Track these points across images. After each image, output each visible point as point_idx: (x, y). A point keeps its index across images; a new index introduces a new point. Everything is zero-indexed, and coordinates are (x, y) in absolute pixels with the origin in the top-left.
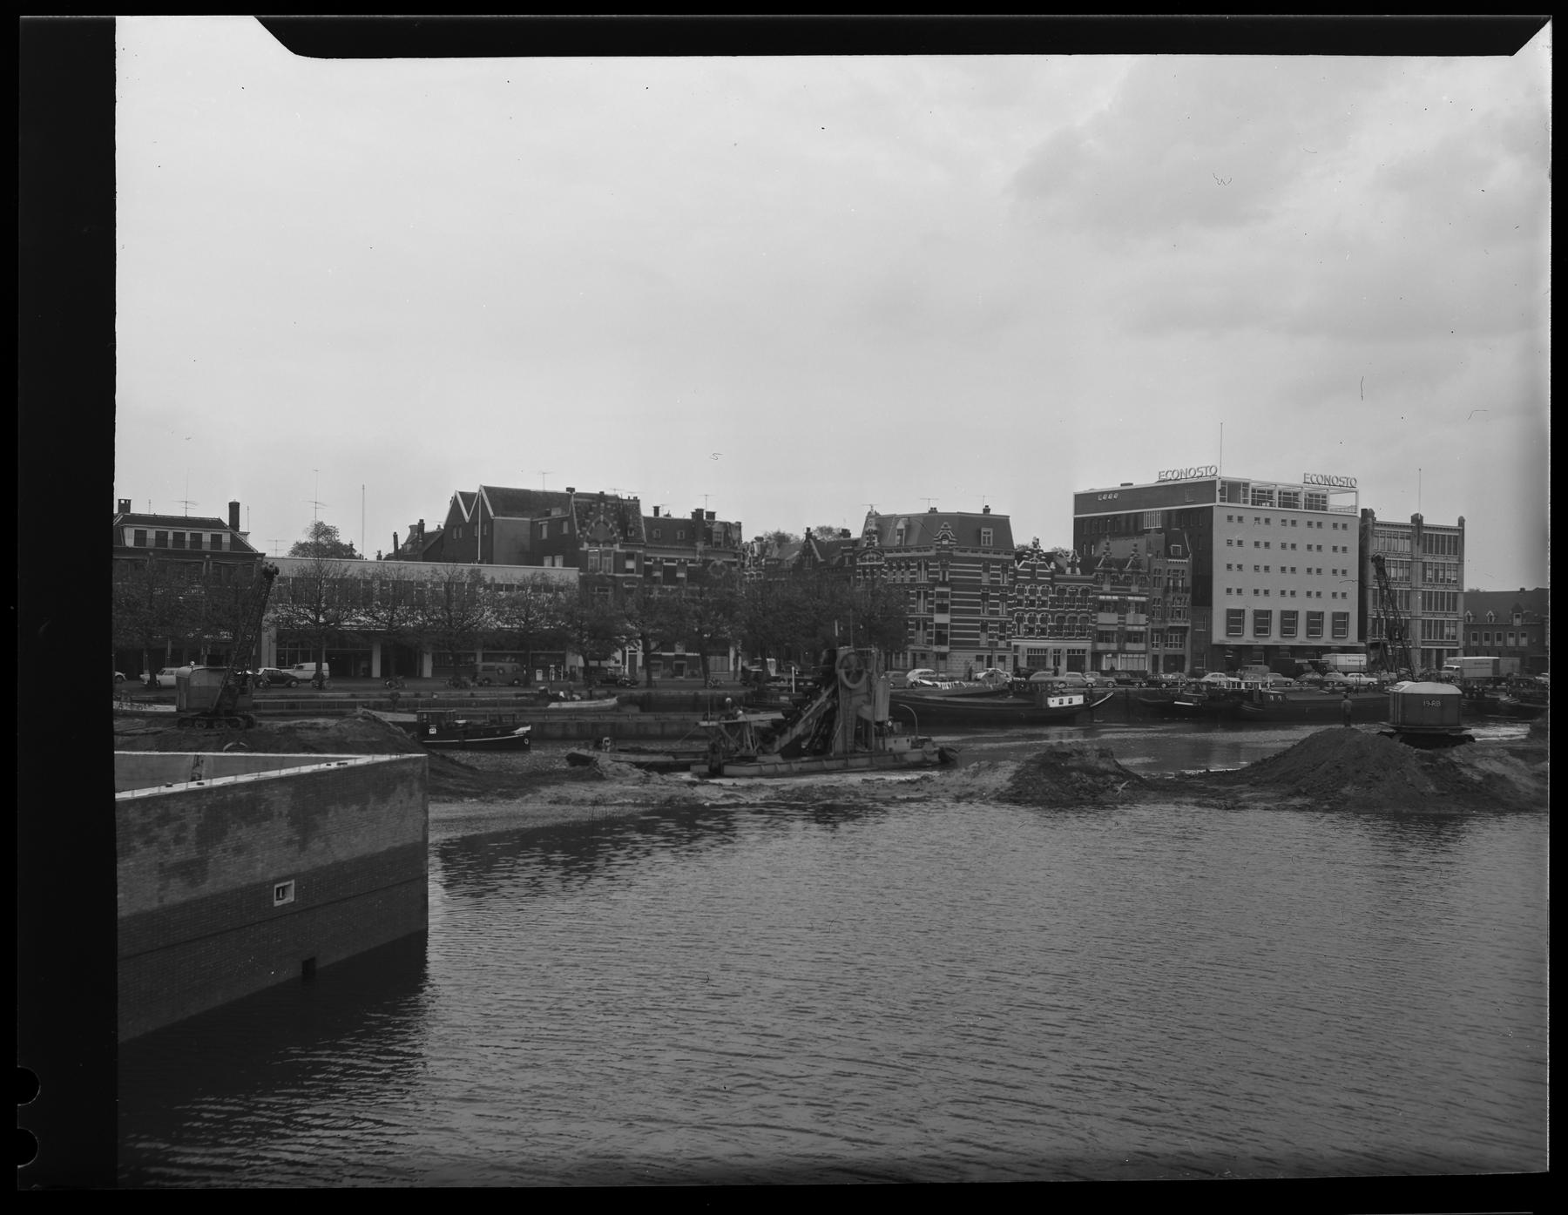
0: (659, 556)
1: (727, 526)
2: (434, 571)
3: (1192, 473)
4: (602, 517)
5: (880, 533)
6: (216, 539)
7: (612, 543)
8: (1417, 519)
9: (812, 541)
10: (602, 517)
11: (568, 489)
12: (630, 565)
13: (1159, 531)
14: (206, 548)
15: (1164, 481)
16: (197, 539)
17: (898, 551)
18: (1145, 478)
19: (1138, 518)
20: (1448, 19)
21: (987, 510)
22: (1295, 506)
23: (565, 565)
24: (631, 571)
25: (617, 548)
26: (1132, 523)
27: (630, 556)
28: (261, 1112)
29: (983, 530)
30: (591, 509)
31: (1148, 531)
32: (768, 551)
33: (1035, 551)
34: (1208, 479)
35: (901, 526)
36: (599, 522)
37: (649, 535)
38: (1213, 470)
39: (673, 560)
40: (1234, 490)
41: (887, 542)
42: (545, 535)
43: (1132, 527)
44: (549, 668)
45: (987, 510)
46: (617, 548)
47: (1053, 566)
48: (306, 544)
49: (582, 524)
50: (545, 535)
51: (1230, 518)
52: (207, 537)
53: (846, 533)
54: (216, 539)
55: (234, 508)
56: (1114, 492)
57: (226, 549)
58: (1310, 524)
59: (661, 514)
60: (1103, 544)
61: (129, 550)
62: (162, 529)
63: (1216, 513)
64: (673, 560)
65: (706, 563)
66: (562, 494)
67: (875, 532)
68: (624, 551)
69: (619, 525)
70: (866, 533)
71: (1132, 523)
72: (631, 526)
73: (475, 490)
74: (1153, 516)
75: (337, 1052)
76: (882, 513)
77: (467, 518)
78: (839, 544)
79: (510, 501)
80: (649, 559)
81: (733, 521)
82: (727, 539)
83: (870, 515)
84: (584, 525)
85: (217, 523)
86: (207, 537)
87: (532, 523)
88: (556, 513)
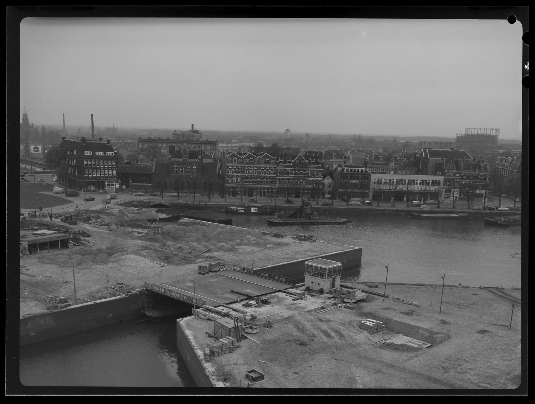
0: (465, 173)
4: (451, 164)
7: (453, 170)
10: (451, 164)
12: (458, 175)
20: (164, 394)
24: (457, 177)
25: (454, 171)
27: (458, 173)
28: (231, 275)
33: (512, 21)
36: (450, 165)
37: (464, 167)
39: (469, 174)
44: (315, 197)
46: (454, 171)
48: (175, 149)
49: (446, 165)
61: (345, 173)
62: (347, 168)
64: (469, 174)
65: (478, 175)
68: (456, 172)
72: (459, 165)
75: (475, 211)
80: (463, 174)
84: (446, 165)
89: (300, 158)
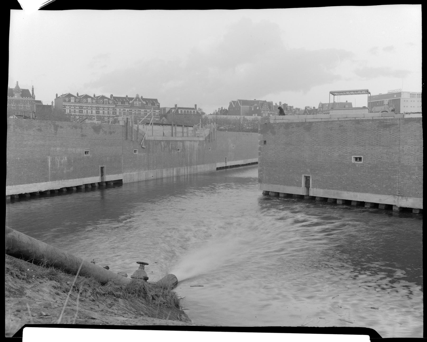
1: (291, 107)
2: (236, 117)
3: (396, 91)
5: (322, 107)
6: (194, 112)
8: (127, 96)
9: (307, 110)
11: (255, 100)
13: (387, 105)
14: (192, 113)
15: (389, 93)
16: (191, 112)
17: (327, 111)
18: (385, 92)
19: (383, 102)
21: (347, 101)
22: (415, 97)
23: (258, 115)
25: (268, 112)
26: (381, 103)
29: (346, 106)
30: (263, 104)
31: (384, 105)
32: (296, 112)
34: (399, 92)
35: (327, 105)
37: (275, 109)
38: (401, 90)
40: (167, 108)
41: (323, 109)
42: (253, 109)
43: (382, 104)
45: (347, 101)
46: (268, 112)
47: (399, 137)
50: (253, 109)
51: (405, 101)
52: (192, 111)
53: (314, 108)
54: (194, 112)
55: (196, 105)
56: (377, 96)
57: (196, 113)
58: (411, 101)
59: (223, 109)
60: (374, 108)
63: (401, 100)
66: (253, 101)
67: (321, 107)
69: (269, 107)
70: (319, 107)
71: (381, 103)
72: (271, 107)
73: (236, 100)
74: (386, 102)
76: (323, 103)
77: (234, 107)
78: (313, 110)
79: (245, 102)
81: (291, 106)
82: (290, 109)
83: (320, 103)
84: (262, 107)
85: (193, 109)
86: (192, 111)
87: (250, 107)
88: (256, 105)
89: (138, 99)
